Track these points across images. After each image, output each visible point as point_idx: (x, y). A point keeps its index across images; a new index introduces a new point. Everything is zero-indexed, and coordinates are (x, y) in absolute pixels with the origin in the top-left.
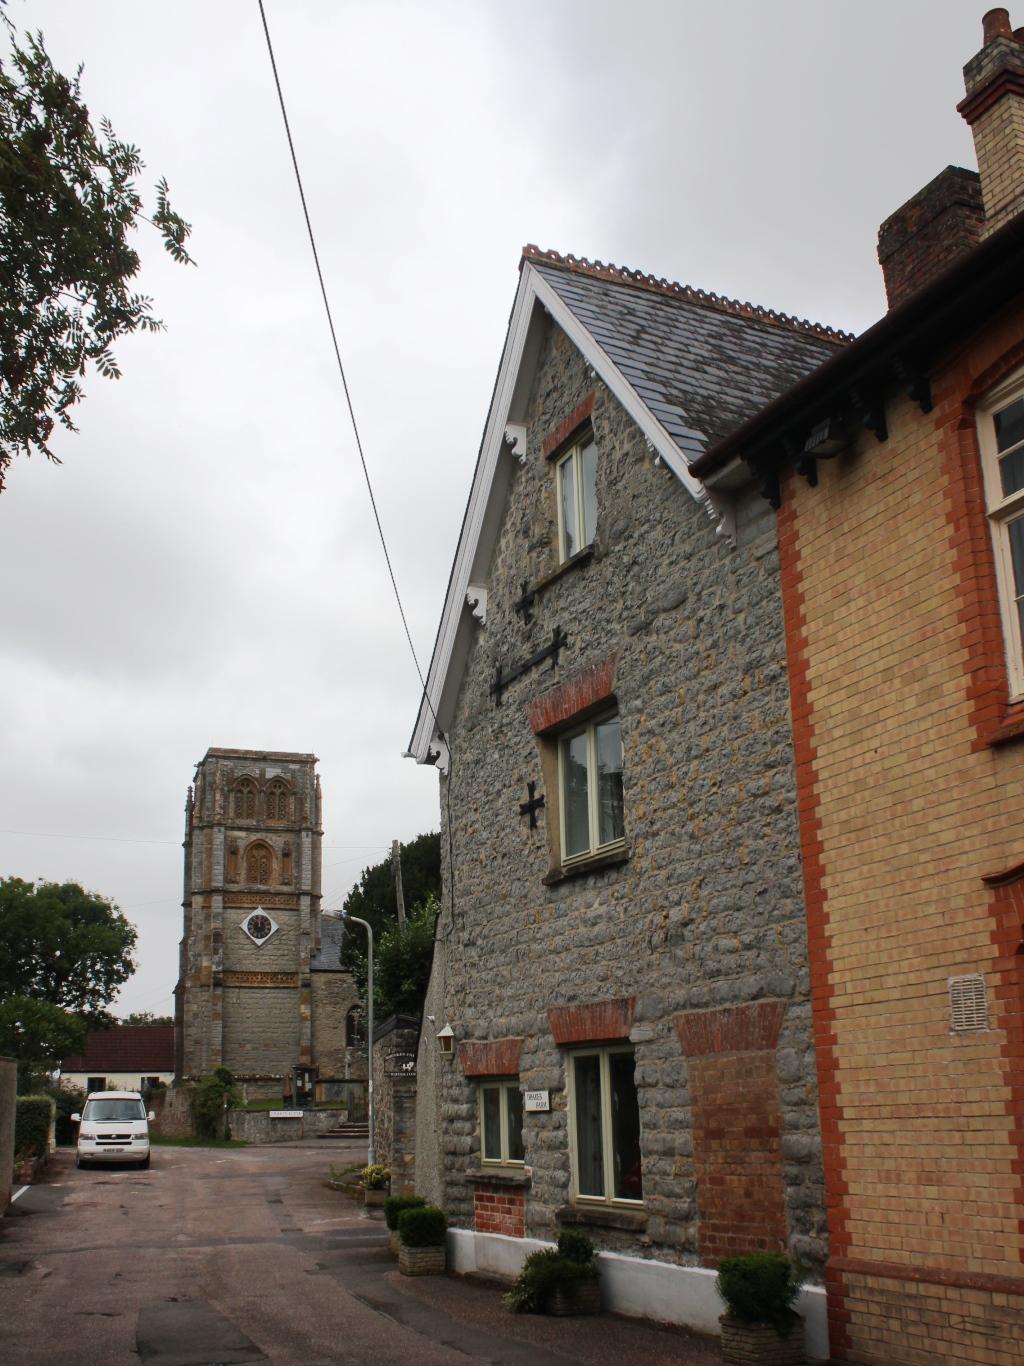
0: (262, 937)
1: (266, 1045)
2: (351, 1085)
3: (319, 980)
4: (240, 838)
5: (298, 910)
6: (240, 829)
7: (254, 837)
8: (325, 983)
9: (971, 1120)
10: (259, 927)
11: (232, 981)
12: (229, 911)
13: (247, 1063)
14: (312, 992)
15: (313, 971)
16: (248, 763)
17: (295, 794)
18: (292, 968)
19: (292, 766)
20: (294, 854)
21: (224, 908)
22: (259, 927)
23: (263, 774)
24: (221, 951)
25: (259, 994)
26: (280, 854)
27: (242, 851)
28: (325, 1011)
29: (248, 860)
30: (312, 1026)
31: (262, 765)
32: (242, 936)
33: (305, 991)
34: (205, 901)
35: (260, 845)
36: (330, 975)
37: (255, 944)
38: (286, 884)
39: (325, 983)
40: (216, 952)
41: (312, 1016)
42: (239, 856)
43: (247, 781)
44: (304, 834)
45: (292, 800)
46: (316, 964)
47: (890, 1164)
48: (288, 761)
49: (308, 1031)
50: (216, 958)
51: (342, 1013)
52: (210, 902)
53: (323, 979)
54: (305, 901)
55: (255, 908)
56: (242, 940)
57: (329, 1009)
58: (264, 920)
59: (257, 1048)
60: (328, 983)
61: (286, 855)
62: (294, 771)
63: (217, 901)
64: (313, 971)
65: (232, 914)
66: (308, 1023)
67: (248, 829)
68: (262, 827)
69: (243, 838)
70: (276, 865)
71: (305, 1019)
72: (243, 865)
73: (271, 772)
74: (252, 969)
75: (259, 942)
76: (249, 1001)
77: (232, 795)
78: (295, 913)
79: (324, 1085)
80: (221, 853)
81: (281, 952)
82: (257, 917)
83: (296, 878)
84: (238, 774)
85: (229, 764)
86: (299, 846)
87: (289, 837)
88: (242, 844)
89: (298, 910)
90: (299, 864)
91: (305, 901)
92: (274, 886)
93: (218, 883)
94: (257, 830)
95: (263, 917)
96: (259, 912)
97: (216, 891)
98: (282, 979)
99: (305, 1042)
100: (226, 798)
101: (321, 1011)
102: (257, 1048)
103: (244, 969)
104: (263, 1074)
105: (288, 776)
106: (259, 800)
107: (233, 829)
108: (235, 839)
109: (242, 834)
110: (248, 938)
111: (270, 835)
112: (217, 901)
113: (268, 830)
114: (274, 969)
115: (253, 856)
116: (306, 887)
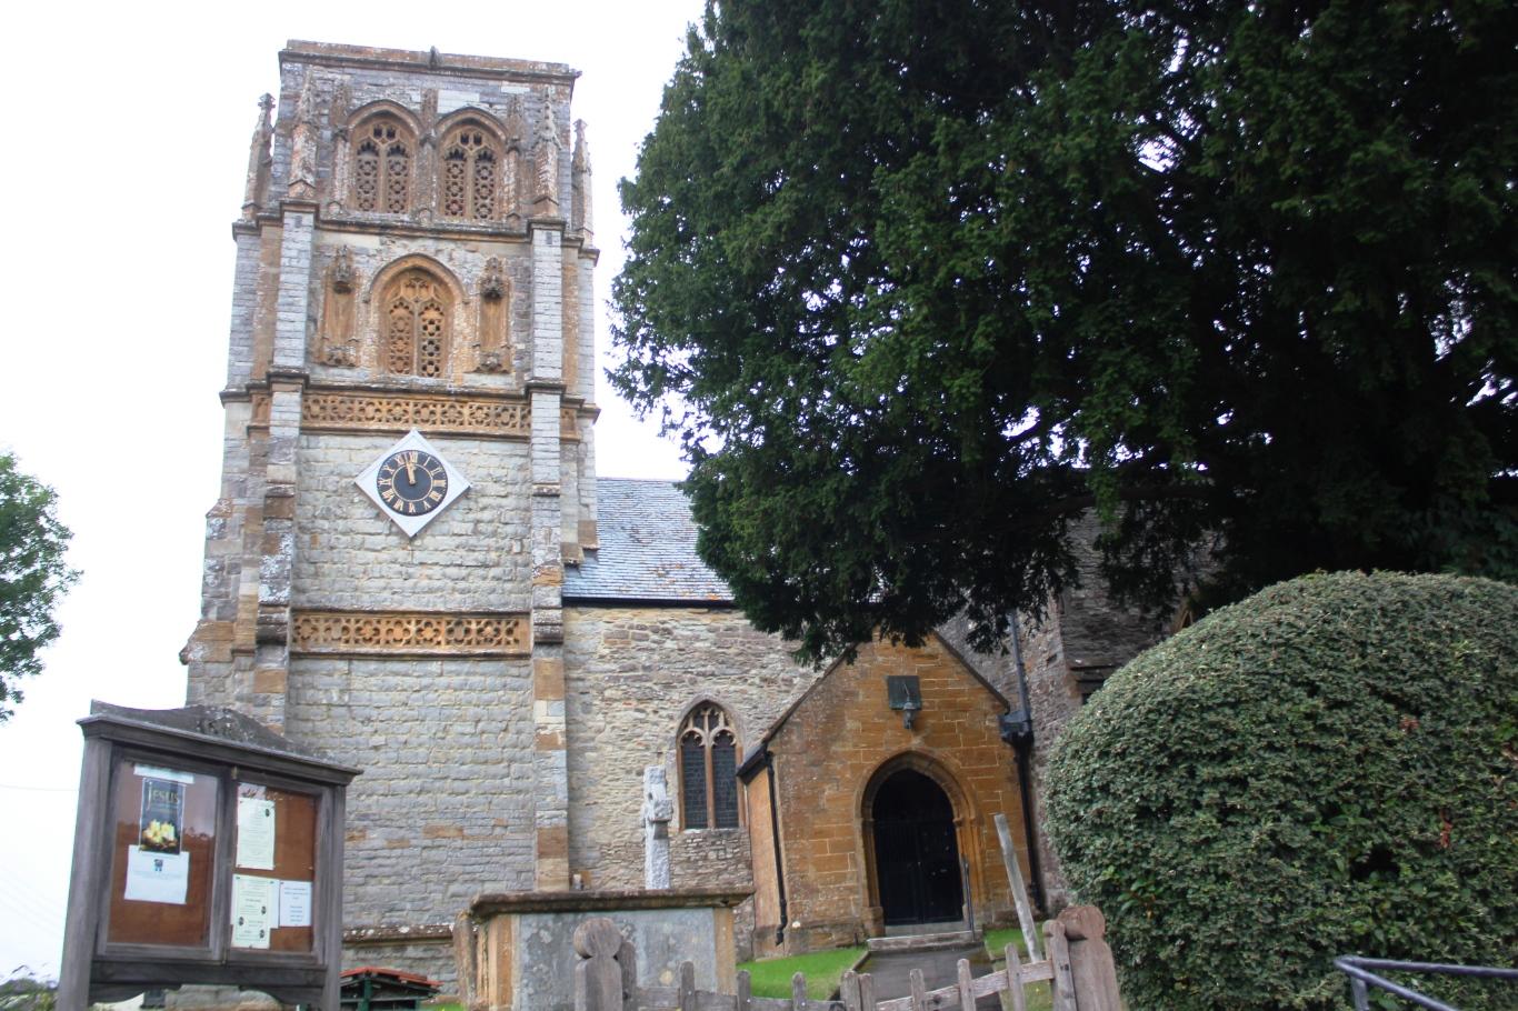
0: (420, 512)
1: (432, 832)
2: (668, 924)
3: (591, 629)
4: (363, 251)
5: (525, 440)
6: (363, 228)
7: (400, 249)
8: (609, 638)
9: (353, 453)
10: (414, 485)
11: (326, 638)
12: (324, 440)
13: (372, 889)
14: (568, 665)
15: (570, 602)
16: (389, 77)
17: (515, 148)
18: (513, 602)
19: (508, 88)
20: (514, 296)
21: (304, 430)
22: (414, 485)
23: (430, 102)
24: (287, 543)
25: (415, 675)
26: (474, 295)
27: (365, 284)
28: (610, 721)
29: (385, 313)
30: (570, 768)
31: (429, 82)
32: (359, 511)
33: (545, 657)
34: (255, 415)
35: (421, 273)
36: (625, 616)
37: (401, 533)
38: (492, 370)
39: (609, 638)
40: (270, 545)
41: (569, 735)
42: (359, 296)
43: (387, 119)
44: (539, 236)
45: (508, 167)
46: (580, 586)
47: (1400, 912)
48: (499, 75)
49: (560, 780)
50: (272, 565)
51: (665, 724)
52: (266, 417)
53: (603, 628)
54: (546, 409)
55: (401, 433)
56: (360, 518)
57: (625, 715)
58: (428, 464)
59: (402, 843)
60: (619, 638)
61: (492, 296)
62: (515, 99)
63: (286, 406)
64: (570, 602)
65: (332, 451)
66: (559, 758)
67: (383, 229)
68: (425, 224)
69: (370, 253)
70: (463, 322)
71: (547, 743)
72: (368, 324)
73: (453, 98)
74: (390, 602)
75: (411, 525)
76: (381, 698)
77: (344, 151)
78: (520, 448)
79: (521, 928)
80: (303, 279)
81: (480, 556)
82: (406, 455)
83: (521, 355)
84: (361, 98)
85: (338, 76)
86: (527, 279)
87: (499, 250)
88: (366, 269)
89: (525, 440)
90: (526, 318)
91: (546, 409)
92: (459, 373)
93: (291, 355)
94: (412, 232)
95: (422, 457)
96: (414, 442)
97: (286, 376)
98: (485, 633)
99: (551, 816)
100: (325, 154)
101: (598, 721)
102: (402, 843)
103: (366, 603)
104: (423, 921)
105: (500, 111)
106: (424, 168)
107: (341, 226)
108: (346, 254)
109: (370, 242)
110: (380, 515)
111: (447, 246)
112: (286, 406)
113: (439, 233)
114: (455, 603)
115: (401, 304)
116: (548, 371)
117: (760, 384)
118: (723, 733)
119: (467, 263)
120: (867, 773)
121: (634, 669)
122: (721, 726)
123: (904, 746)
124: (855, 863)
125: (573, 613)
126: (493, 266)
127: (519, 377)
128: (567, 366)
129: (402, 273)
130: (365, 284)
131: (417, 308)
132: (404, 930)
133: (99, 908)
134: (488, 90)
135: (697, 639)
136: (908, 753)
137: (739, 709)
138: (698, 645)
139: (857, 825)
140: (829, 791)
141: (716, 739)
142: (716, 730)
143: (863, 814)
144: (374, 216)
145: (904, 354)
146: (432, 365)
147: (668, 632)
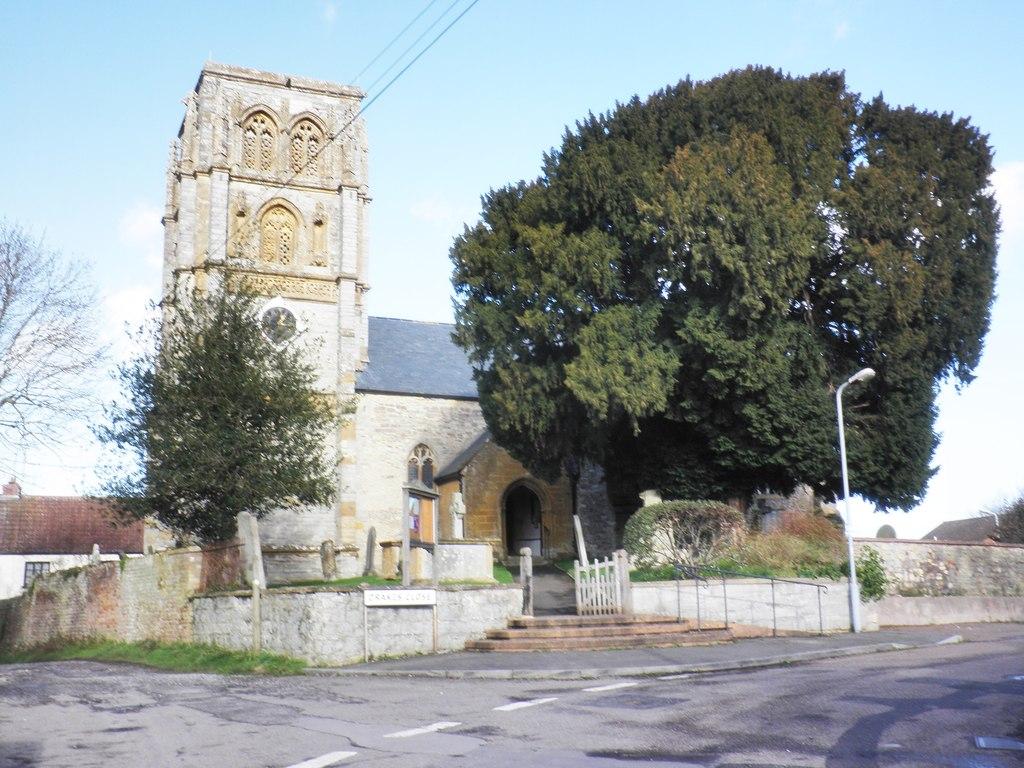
8: (376, 410)
27: (253, 212)
90: (339, 237)
108: (243, 195)
116: (349, 270)
117: (842, 98)
118: (428, 460)
119: (305, 202)
120: (505, 487)
121: (387, 425)
122: (427, 456)
123: (522, 475)
124: (498, 528)
125: (360, 396)
126: (320, 207)
127: (332, 269)
128: (359, 266)
129: (271, 208)
130: (253, 212)
131: (277, 226)
132: (274, 548)
133: (359, 242)
134: (316, 100)
135: (418, 412)
136: (523, 479)
137: (437, 448)
138: (418, 415)
139: (499, 510)
140: (487, 494)
141: (425, 462)
142: (425, 457)
143: (502, 505)
144: (251, 172)
145: (748, 188)
146: (284, 260)
147: (403, 408)
